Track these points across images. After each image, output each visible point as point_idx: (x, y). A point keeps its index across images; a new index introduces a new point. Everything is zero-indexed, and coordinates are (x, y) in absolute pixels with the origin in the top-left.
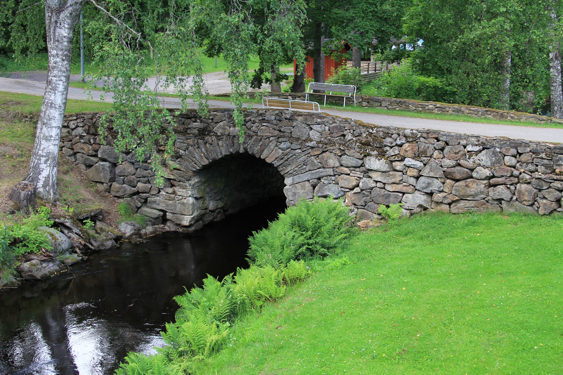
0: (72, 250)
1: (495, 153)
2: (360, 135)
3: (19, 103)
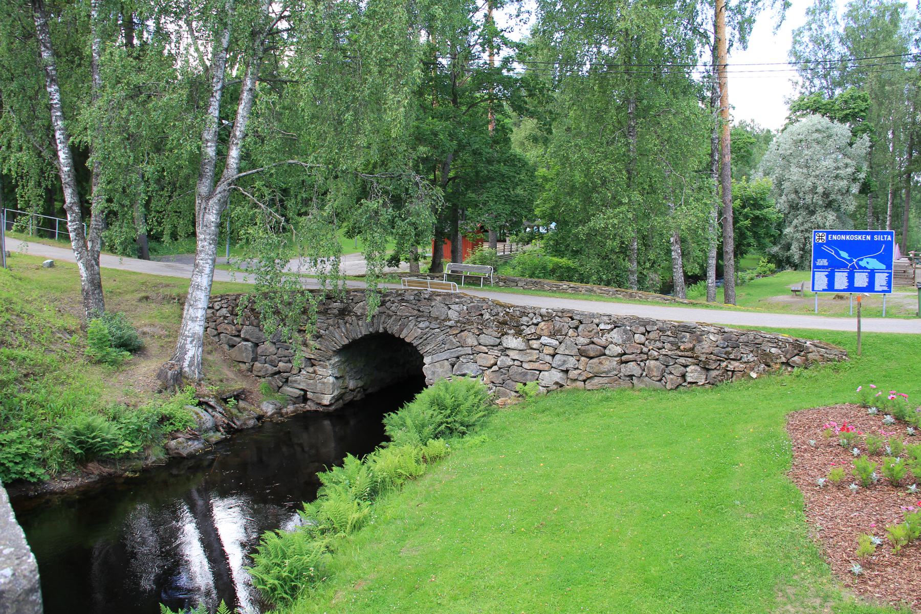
0: (216, 428)
1: (625, 331)
2: (497, 314)
3: (168, 286)
